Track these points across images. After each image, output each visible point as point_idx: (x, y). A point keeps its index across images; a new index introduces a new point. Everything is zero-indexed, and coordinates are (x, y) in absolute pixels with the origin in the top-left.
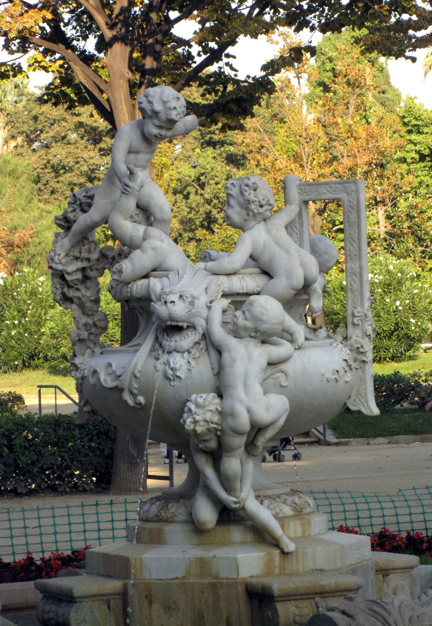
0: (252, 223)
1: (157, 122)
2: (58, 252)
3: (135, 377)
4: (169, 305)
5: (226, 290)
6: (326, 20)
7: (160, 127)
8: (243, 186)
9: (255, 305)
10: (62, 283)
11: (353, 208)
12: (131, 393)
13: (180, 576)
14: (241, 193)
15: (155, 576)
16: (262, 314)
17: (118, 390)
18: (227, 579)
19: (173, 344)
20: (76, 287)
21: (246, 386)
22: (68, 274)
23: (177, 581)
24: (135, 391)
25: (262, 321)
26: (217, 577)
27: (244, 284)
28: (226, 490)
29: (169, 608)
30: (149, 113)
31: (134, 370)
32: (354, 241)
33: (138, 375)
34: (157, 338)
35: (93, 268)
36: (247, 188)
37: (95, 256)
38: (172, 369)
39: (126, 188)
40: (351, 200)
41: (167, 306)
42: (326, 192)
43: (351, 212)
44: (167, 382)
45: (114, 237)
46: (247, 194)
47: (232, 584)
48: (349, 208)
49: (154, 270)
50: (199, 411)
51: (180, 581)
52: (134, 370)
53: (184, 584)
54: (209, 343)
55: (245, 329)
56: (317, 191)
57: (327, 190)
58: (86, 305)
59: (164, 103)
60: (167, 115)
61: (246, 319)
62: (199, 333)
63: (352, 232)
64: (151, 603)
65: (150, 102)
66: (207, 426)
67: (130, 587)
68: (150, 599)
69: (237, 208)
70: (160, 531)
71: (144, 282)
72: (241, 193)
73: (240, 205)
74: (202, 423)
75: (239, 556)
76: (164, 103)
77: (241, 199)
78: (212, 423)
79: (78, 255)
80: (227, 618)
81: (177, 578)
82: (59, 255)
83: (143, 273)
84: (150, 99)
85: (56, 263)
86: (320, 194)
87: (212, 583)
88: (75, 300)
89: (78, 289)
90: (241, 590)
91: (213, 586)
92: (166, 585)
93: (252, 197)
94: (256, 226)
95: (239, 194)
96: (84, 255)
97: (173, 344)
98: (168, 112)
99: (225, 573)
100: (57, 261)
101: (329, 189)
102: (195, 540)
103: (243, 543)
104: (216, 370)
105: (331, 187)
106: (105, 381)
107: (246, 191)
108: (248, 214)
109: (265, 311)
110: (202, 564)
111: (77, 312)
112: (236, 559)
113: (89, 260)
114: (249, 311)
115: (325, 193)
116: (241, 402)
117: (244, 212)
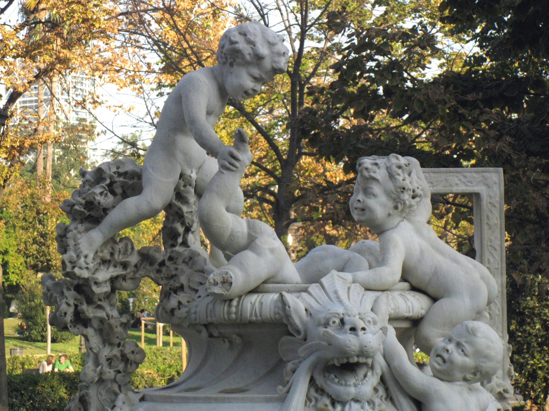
0: (397, 220)
1: (256, 72)
4: (361, 333)
5: (392, 312)
7: (256, 79)
8: (394, 168)
9: (479, 335)
10: (79, 297)
11: (495, 206)
14: (391, 176)
16: (488, 347)
20: (99, 303)
22: (96, 283)
25: (487, 357)
27: (409, 304)
32: (496, 250)
35: (128, 277)
36: (400, 171)
37: (134, 259)
39: (233, 161)
40: (492, 194)
41: (357, 335)
42: (458, 182)
43: (491, 211)
45: (466, 234)
48: (489, 206)
49: (265, 282)
55: (464, 368)
56: (447, 180)
57: (460, 180)
58: (116, 330)
60: (275, 62)
61: (466, 355)
62: (377, 375)
63: (492, 238)
65: (251, 43)
69: (383, 198)
71: (254, 298)
72: (391, 176)
73: (388, 194)
76: (271, 44)
77: (390, 186)
79: (108, 257)
82: (86, 257)
84: (252, 38)
85: (80, 268)
86: (451, 185)
88: (95, 324)
93: (407, 183)
94: (402, 223)
95: (387, 177)
96: (119, 258)
98: (276, 59)
100: (84, 265)
101: (462, 178)
105: (465, 177)
107: (398, 174)
108: (396, 208)
109: (491, 344)
111: (95, 341)
113: (125, 265)
114: (471, 344)
115: (457, 184)
117: (391, 204)
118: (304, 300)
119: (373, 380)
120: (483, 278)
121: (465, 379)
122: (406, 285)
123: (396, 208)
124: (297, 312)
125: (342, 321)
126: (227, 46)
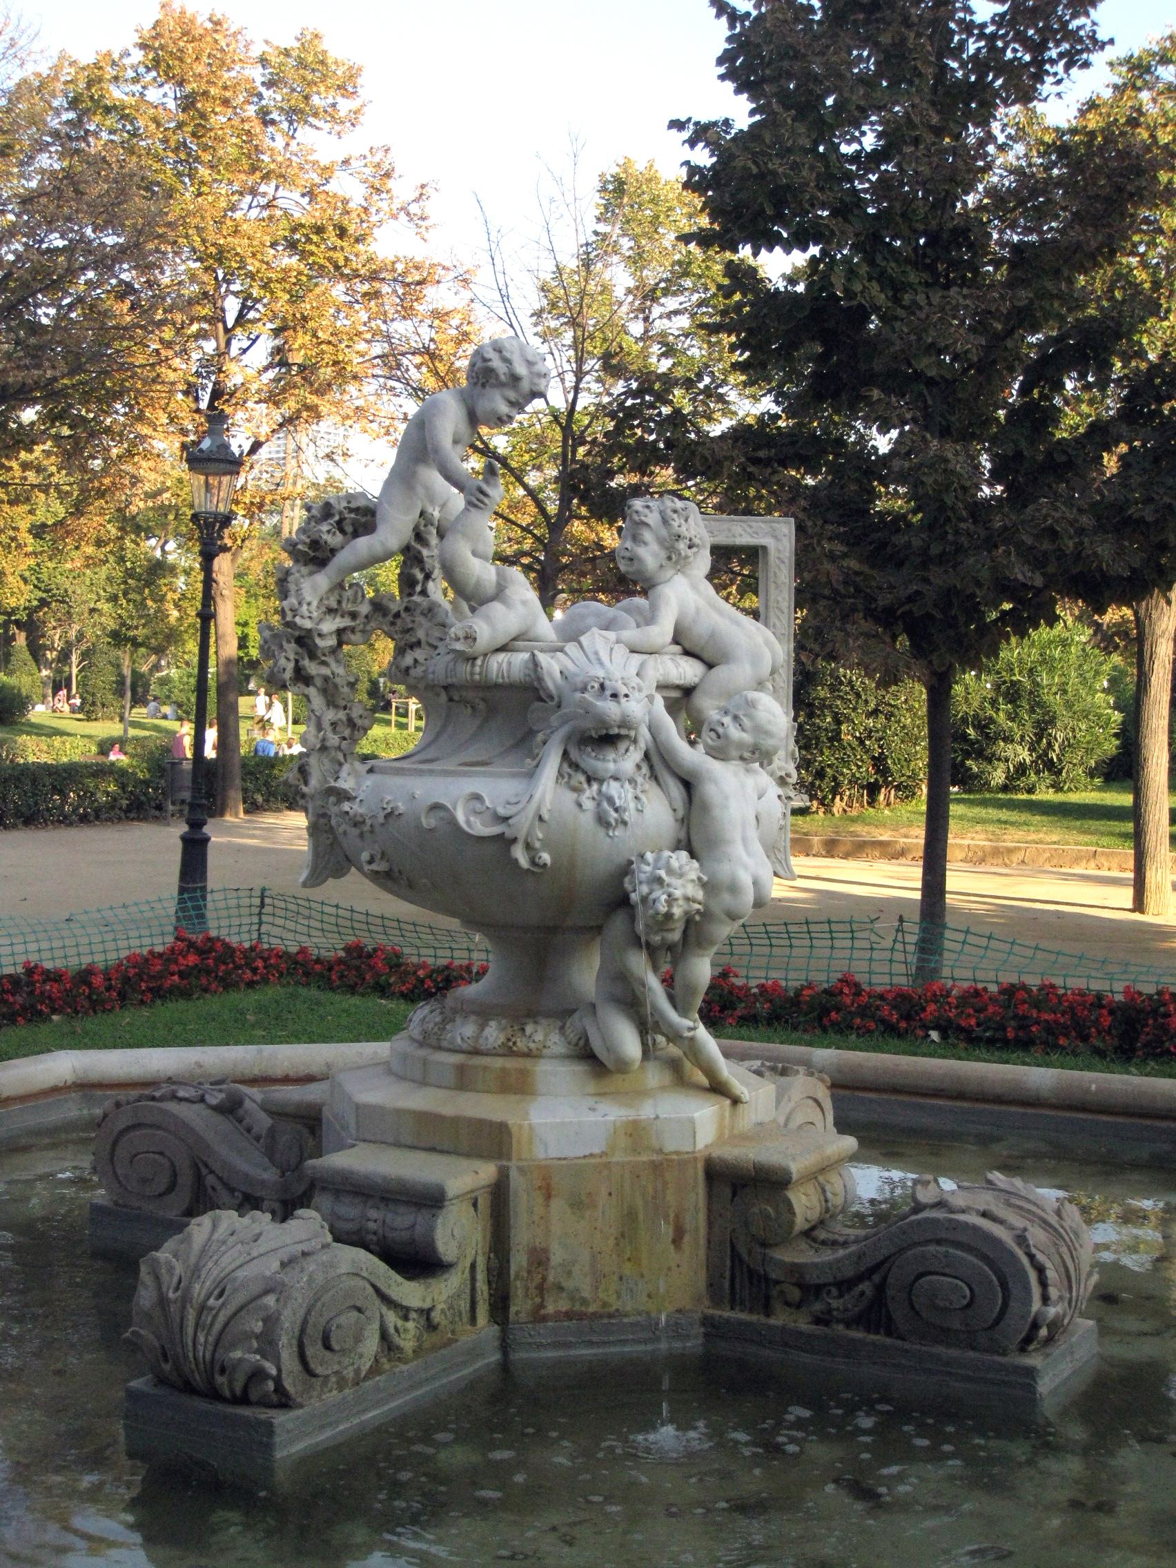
0: (670, 573)
2: (308, 599)
3: (541, 819)
4: (623, 700)
6: (57, 319)
8: (669, 512)
12: (528, 846)
13: (597, 1151)
15: (553, 1153)
17: (504, 842)
18: (677, 1153)
19: (611, 766)
21: (744, 840)
22: (320, 635)
23: (593, 1161)
24: (537, 845)
25: (768, 733)
26: (660, 1151)
28: (675, 1007)
29: (578, 1205)
30: (503, 378)
31: (539, 808)
33: (546, 816)
34: (565, 754)
37: (365, 609)
38: (616, 810)
44: (601, 832)
46: (675, 524)
47: (682, 1163)
50: (676, 882)
51: (598, 1160)
52: (539, 808)
53: (608, 1165)
54: (658, 762)
59: (530, 364)
64: (548, 1197)
65: (507, 361)
66: (686, 907)
67: (514, 1174)
68: (548, 1195)
69: (654, 547)
70: (524, 1073)
72: (665, 521)
73: (661, 541)
74: (681, 902)
75: (696, 1115)
76: (530, 364)
77: (663, 532)
78: (694, 901)
79: (335, 605)
80: (677, 1216)
81: (591, 1155)
83: (501, 641)
84: (508, 355)
87: (653, 1162)
88: (318, 682)
89: (324, 663)
90: (700, 1167)
91: (657, 1168)
92: (575, 1168)
97: (611, 766)
98: (536, 380)
99: (673, 1143)
100: (306, 614)
102: (591, 1087)
103: (663, 1088)
104: (681, 813)
106: (468, 822)
108: (669, 558)
110: (635, 1132)
112: (692, 1121)
113: (354, 615)
116: (746, 867)
118: (558, 661)
119: (635, 756)
120: (767, 643)
121: (742, 758)
122: (677, 648)
123: (669, 558)
124: (550, 674)
125: (602, 687)
126: (479, 364)
